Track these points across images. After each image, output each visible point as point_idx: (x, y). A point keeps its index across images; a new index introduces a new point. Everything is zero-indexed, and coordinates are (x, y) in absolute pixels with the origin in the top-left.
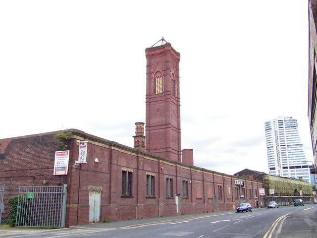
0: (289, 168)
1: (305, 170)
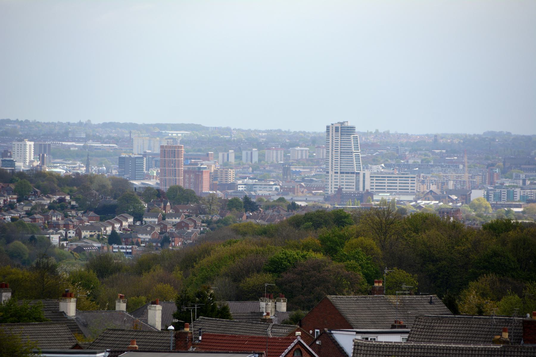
0: (339, 173)
1: (351, 176)
